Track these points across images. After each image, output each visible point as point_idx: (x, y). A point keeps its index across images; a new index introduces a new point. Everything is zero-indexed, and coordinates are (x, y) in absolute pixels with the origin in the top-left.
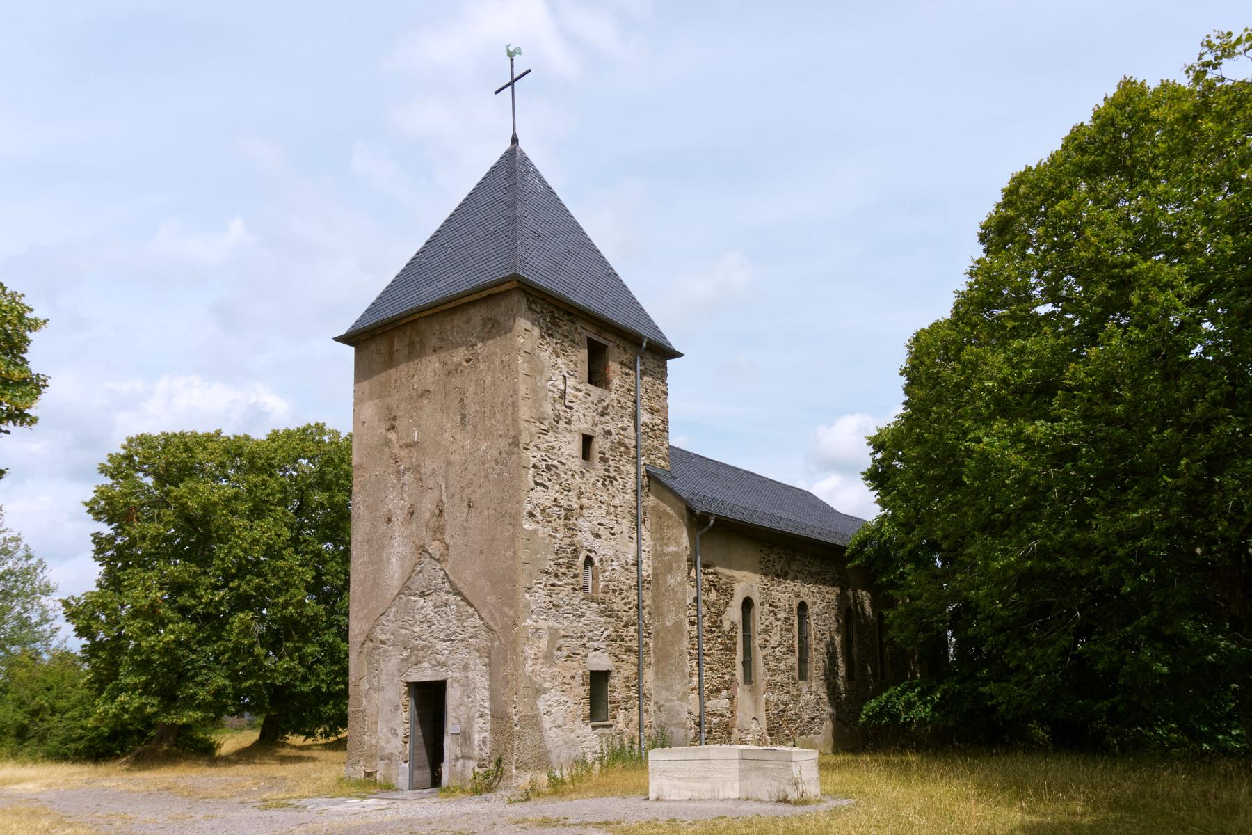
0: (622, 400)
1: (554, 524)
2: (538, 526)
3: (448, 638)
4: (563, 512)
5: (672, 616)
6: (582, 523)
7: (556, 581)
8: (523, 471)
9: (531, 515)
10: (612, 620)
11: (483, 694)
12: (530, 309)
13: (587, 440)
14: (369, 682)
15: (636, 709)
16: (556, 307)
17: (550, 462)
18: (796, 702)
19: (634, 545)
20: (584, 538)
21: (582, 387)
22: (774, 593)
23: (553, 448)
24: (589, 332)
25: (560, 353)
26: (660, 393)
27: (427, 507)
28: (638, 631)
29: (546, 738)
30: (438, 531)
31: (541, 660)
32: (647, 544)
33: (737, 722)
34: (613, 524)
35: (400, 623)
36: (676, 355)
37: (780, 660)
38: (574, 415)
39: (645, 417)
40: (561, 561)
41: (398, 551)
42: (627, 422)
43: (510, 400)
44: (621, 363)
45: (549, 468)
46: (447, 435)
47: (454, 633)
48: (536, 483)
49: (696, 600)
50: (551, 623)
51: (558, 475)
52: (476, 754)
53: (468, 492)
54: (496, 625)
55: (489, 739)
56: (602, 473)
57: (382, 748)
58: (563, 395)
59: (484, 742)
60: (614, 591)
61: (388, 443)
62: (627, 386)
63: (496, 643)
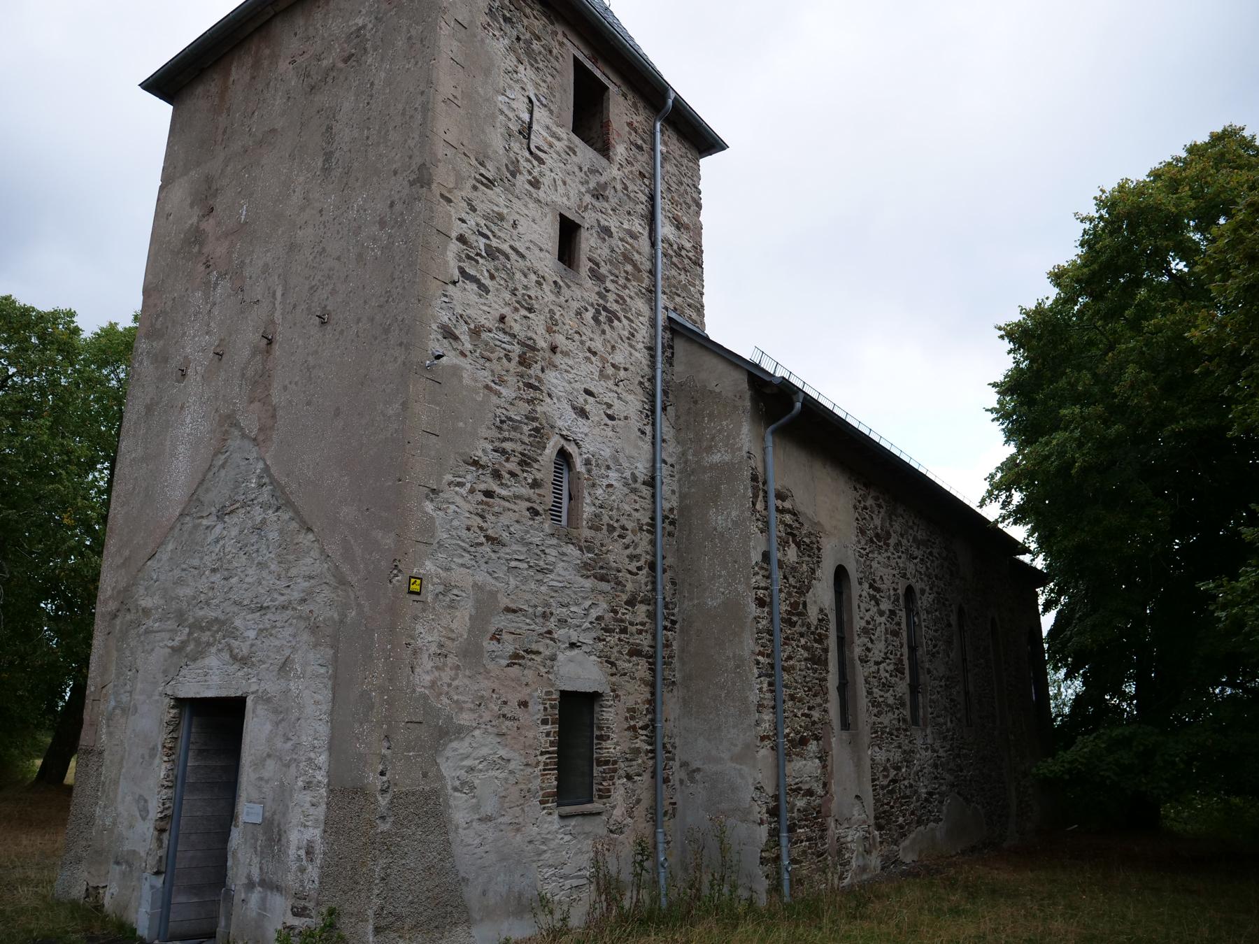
0: (631, 187)
1: (497, 367)
2: (461, 361)
4: (517, 349)
7: (495, 487)
8: (436, 240)
9: (449, 334)
10: (604, 586)
11: (314, 730)
13: (568, 231)
17: (495, 243)
18: (909, 763)
19: (647, 447)
20: (559, 413)
22: (875, 564)
23: (501, 217)
28: (652, 615)
30: (260, 383)
32: (670, 451)
33: (834, 806)
34: (609, 397)
37: (886, 686)
39: (665, 229)
40: (508, 446)
41: (191, 423)
42: (638, 226)
43: (420, 99)
45: (492, 253)
48: (462, 272)
49: (766, 556)
50: (481, 577)
51: (511, 275)
55: (319, 848)
56: (594, 298)
58: (526, 131)
59: (310, 852)
60: (611, 529)
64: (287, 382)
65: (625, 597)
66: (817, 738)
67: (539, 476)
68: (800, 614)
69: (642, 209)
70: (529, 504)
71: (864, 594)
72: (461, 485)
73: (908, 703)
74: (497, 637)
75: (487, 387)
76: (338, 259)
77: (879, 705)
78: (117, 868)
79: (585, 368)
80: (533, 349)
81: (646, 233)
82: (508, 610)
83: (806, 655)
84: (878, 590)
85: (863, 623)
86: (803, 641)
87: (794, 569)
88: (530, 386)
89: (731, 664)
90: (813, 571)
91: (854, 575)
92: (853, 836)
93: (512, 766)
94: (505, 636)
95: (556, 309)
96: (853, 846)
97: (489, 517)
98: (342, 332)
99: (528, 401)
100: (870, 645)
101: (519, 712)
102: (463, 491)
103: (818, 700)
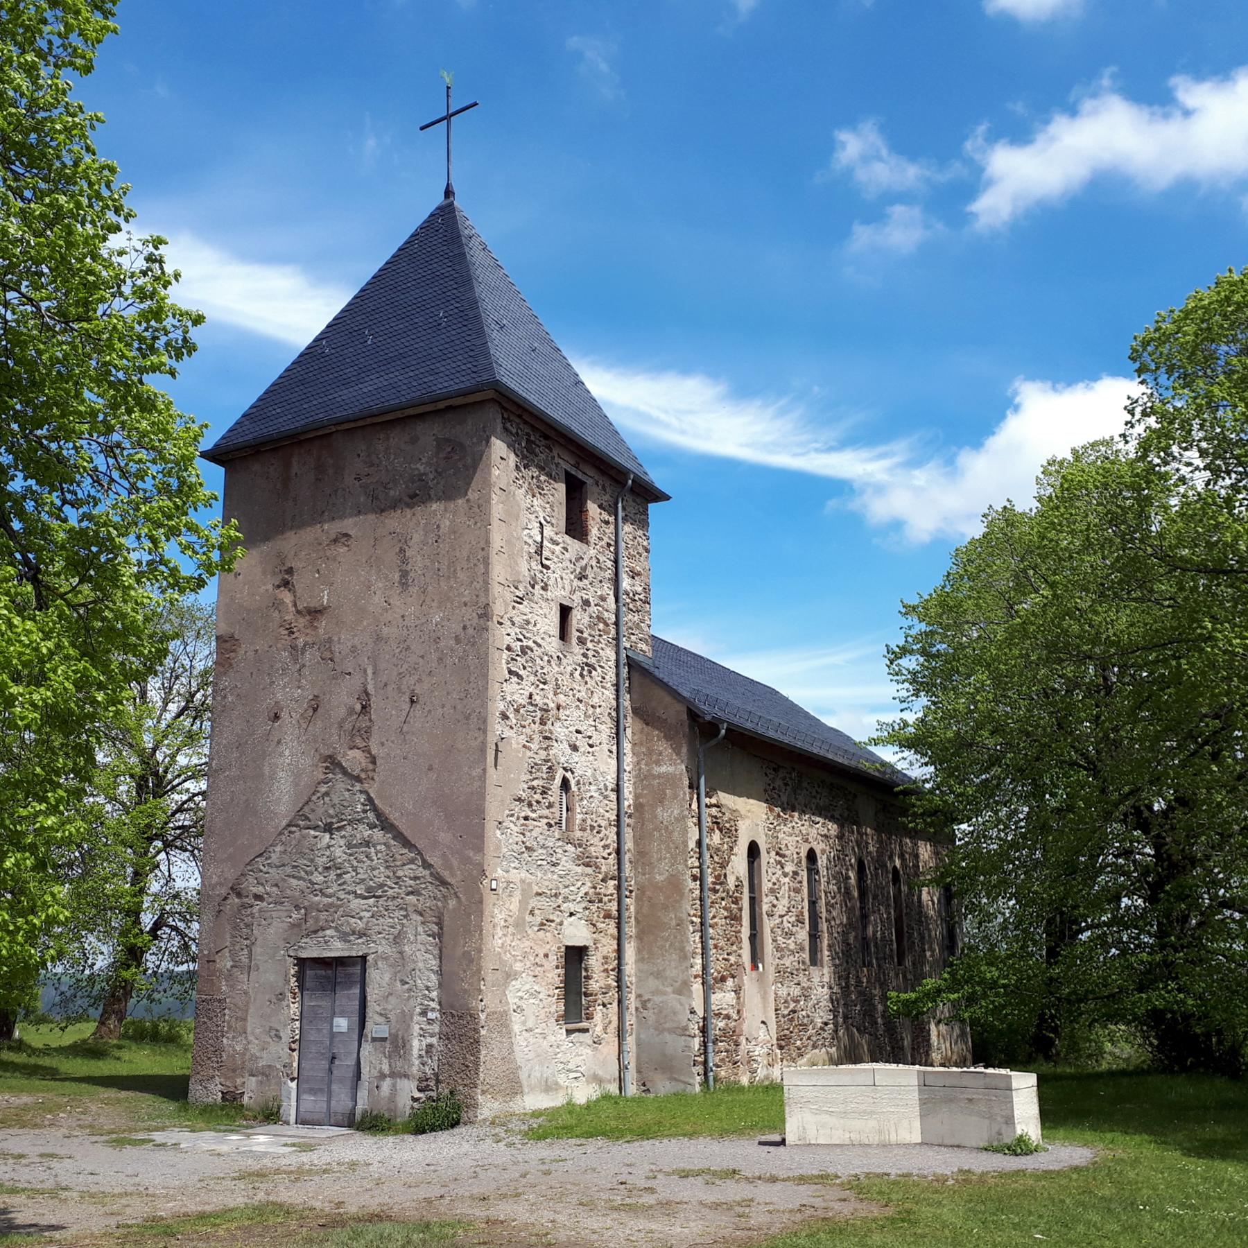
0: (602, 559)
3: (371, 893)
4: (539, 714)
5: (665, 866)
6: (559, 730)
10: (589, 870)
12: (505, 429)
13: (565, 611)
14: (233, 954)
15: (615, 1004)
16: (533, 427)
19: (614, 762)
20: (560, 751)
21: (558, 538)
22: (781, 835)
24: (565, 463)
25: (536, 490)
26: (641, 550)
27: (342, 698)
29: (516, 1048)
30: (359, 735)
31: (511, 929)
33: (745, 1027)
35: (288, 870)
36: (660, 496)
37: (789, 934)
38: (552, 577)
39: (626, 583)
40: (535, 783)
42: (608, 590)
44: (600, 506)
45: (524, 650)
46: (378, 599)
47: (381, 886)
48: (510, 672)
51: (533, 660)
52: (415, 1069)
53: (411, 680)
54: (453, 875)
56: (581, 659)
57: (255, 1058)
60: (592, 828)
61: (277, 605)
62: (606, 540)
63: (452, 903)
64: (384, 740)
65: (601, 876)
66: (733, 977)
67: (552, 799)
68: (721, 884)
69: (609, 574)
70: (546, 821)
71: (772, 861)
72: (512, 815)
73: (807, 948)
74: (532, 913)
75: (524, 746)
76: (422, 657)
77: (782, 950)
78: (254, 1079)
79: (576, 713)
80: (547, 711)
81: (612, 593)
82: (539, 894)
83: (726, 914)
84: (783, 856)
85: (770, 885)
86: (724, 903)
87: (718, 850)
88: (546, 738)
89: (674, 923)
90: (731, 848)
91: (763, 848)
92: (759, 1051)
93: (541, 996)
94: (536, 912)
95: (558, 676)
96: (759, 1059)
97: (528, 834)
98: (429, 711)
99: (546, 749)
100: (775, 902)
101: (544, 961)
102: (513, 819)
103: (734, 948)
